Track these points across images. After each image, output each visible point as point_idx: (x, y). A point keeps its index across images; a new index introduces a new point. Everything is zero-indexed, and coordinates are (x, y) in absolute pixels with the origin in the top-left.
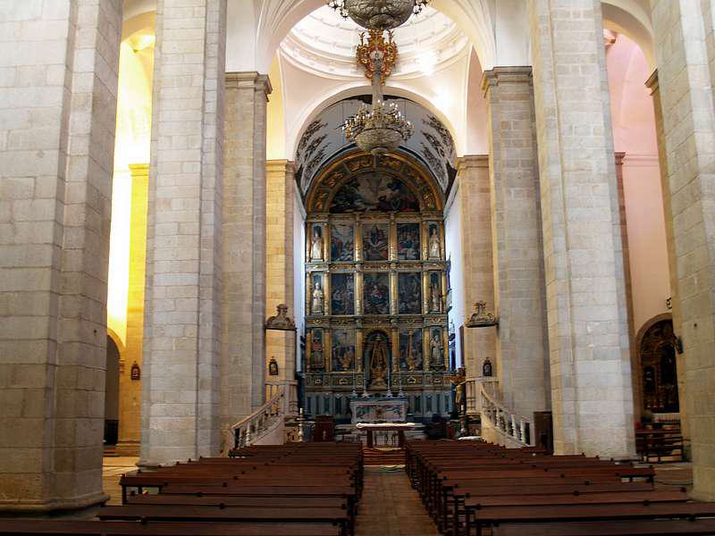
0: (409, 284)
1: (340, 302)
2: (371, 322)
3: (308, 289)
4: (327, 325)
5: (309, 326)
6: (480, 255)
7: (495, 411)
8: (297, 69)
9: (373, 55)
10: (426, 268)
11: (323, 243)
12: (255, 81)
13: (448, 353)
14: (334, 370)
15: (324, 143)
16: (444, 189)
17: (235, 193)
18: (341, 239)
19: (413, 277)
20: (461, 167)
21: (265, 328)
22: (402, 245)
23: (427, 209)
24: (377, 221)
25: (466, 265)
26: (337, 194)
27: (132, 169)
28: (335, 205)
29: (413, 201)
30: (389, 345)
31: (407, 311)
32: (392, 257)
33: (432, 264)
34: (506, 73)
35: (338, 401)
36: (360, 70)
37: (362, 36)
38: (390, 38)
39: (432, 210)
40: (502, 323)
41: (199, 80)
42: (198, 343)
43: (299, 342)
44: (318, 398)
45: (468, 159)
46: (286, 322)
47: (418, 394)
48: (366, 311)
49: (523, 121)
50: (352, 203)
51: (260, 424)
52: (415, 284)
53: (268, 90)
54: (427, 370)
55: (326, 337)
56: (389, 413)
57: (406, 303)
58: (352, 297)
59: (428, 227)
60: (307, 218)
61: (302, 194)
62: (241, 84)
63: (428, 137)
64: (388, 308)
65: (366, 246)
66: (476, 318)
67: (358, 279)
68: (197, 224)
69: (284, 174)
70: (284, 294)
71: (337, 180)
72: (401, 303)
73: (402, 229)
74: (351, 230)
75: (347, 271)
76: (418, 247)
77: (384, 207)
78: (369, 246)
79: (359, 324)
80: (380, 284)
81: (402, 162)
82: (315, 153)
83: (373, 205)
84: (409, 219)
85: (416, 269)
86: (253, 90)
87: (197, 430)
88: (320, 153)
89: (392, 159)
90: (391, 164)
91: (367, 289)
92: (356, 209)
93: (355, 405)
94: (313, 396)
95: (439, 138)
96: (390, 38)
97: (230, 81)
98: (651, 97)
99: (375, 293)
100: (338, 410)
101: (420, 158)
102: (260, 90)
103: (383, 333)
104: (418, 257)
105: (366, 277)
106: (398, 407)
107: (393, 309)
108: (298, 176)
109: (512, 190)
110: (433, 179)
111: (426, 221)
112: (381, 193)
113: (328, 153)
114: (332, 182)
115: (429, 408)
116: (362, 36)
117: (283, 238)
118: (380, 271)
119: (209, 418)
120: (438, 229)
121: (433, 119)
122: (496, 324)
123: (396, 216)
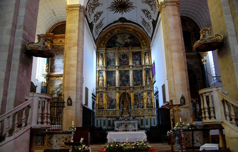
1: (110, 82)
44: (101, 120)
55: (104, 95)
57: (136, 82)
63: (144, 11)
71: (109, 36)
78: (121, 60)
82: (99, 21)
94: (99, 119)
112: (126, 41)
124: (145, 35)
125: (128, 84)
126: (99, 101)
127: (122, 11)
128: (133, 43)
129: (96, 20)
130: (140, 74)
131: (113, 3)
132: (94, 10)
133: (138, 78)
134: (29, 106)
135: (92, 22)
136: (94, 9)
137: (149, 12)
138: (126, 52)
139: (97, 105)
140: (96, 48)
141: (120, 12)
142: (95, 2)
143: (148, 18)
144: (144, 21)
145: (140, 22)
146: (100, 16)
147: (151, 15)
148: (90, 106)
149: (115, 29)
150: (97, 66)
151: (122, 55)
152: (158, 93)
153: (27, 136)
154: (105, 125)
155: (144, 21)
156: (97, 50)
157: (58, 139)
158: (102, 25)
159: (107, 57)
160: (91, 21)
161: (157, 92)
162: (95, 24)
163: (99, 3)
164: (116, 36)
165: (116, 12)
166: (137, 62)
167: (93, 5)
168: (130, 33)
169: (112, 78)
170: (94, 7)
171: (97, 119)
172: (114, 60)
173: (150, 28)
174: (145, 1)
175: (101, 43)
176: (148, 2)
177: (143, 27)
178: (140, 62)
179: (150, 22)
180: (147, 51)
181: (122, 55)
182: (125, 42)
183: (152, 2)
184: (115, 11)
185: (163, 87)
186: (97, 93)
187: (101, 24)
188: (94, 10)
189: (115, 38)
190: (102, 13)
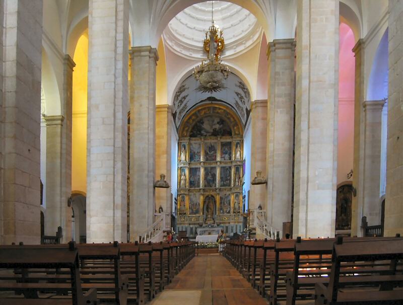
0: (226, 171)
1: (193, 181)
2: (207, 191)
3: (179, 175)
4: (187, 193)
5: (179, 193)
6: (261, 152)
7: (263, 226)
8: (172, 52)
10: (234, 164)
11: (186, 153)
12: (150, 52)
13: (241, 205)
14: (190, 214)
15: (187, 99)
16: (244, 123)
18: (195, 150)
19: (227, 169)
20: (253, 107)
21: (155, 187)
22: (223, 153)
23: (235, 134)
24: (211, 141)
26: (193, 128)
29: (229, 130)
30: (215, 202)
31: (224, 185)
32: (218, 159)
33: (236, 162)
34: (280, 43)
35: (192, 229)
37: (206, 34)
38: (221, 35)
39: (237, 134)
40: (269, 182)
41: (113, 33)
42: (114, 185)
43: (174, 200)
45: (257, 102)
46: (164, 183)
47: (227, 225)
48: (205, 186)
50: (200, 132)
51: (151, 234)
52: (228, 172)
53: (156, 59)
54: (232, 214)
55: (187, 198)
58: (199, 179)
59: (235, 144)
60: (179, 140)
61: (176, 127)
62: (143, 53)
63: (238, 94)
64: (215, 184)
65: (206, 154)
66: (257, 179)
67: (202, 171)
68: (113, 118)
69: (166, 112)
71: (193, 120)
72: (221, 181)
73: (223, 145)
74: (198, 145)
75: (196, 167)
76: (230, 154)
77: (215, 134)
79: (202, 192)
81: (224, 110)
82: (183, 105)
83: (210, 133)
84: (227, 139)
85: (229, 165)
86: (148, 57)
87: (114, 230)
88: (185, 105)
89: (220, 109)
90: (219, 111)
91: (206, 174)
92: (202, 135)
93: (199, 230)
95: (243, 94)
96: (221, 35)
97: (135, 53)
98: (354, 58)
99: (209, 177)
100: (191, 232)
101: (234, 108)
102: (152, 57)
103: (212, 196)
104: (230, 158)
105: (206, 169)
106: (218, 231)
108: (174, 115)
110: (240, 120)
111: (235, 140)
112: (214, 127)
113: (190, 105)
114: (191, 121)
115: (232, 231)
116: (206, 34)
118: (212, 166)
119: (120, 224)
120: (240, 144)
121: (240, 83)
122: (266, 183)
123: (221, 138)
126: (180, 206)
161: (245, 196)
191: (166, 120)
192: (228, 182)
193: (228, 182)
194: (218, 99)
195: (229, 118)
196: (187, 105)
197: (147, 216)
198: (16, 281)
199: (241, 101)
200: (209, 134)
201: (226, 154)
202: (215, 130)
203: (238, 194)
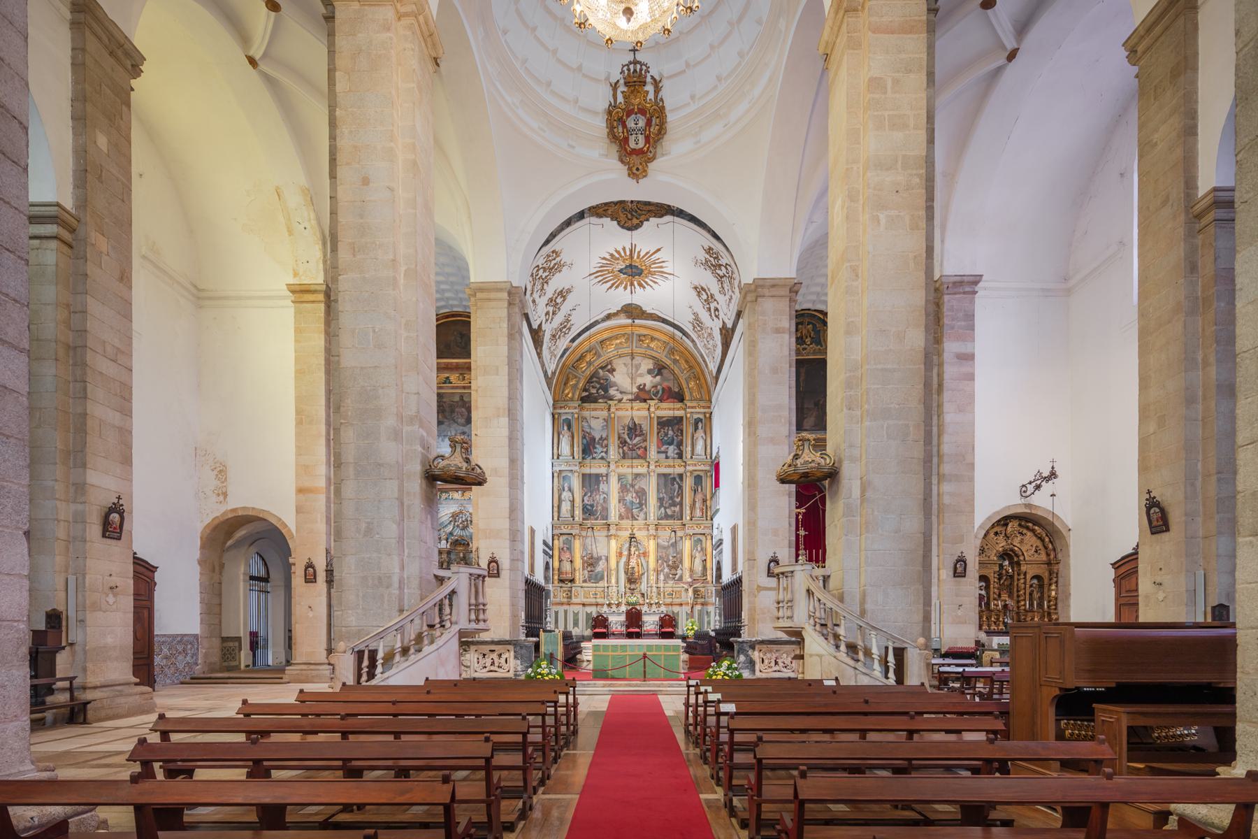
1: (592, 506)
5: (556, 532)
9: (630, 123)
14: (585, 581)
15: (571, 300)
17: (361, 216)
18: (593, 433)
19: (674, 479)
25: (749, 435)
26: (589, 381)
27: (293, 292)
28: (587, 393)
36: (614, 145)
43: (539, 547)
44: (566, 612)
49: (912, 76)
50: (606, 390)
55: (577, 544)
56: (567, 567)
57: (665, 508)
61: (545, 373)
63: (699, 290)
66: (799, 462)
70: (507, 470)
71: (590, 364)
72: (660, 508)
78: (626, 442)
80: (636, 487)
82: (559, 318)
85: (680, 470)
94: (561, 609)
104: (680, 456)
107: (652, 515)
109: (882, 217)
111: (692, 410)
112: (640, 381)
117: (506, 394)
118: (636, 471)
124: (699, 364)
125: (642, 515)
126: (560, 561)
127: (632, 284)
128: (663, 389)
129: (553, 314)
130: (676, 486)
131: (604, 258)
132: (545, 285)
133: (671, 498)
134: (453, 592)
135: (540, 326)
136: (546, 281)
137: (712, 297)
138: (640, 418)
139: (556, 572)
140: (551, 402)
141: (625, 288)
142: (551, 261)
143: (711, 315)
144: (697, 319)
145: (685, 321)
146: (564, 301)
147: (719, 307)
148: (539, 578)
149: (610, 339)
150: (555, 457)
151: (628, 426)
152: (721, 544)
153: (454, 644)
154: (578, 627)
155: (697, 322)
156: (554, 408)
157: (481, 657)
158: (569, 329)
159: (583, 431)
160: (538, 322)
161: (720, 542)
162: (548, 329)
163: (562, 263)
164: (610, 363)
165: (613, 288)
166: (671, 448)
167: (544, 271)
168: (654, 354)
169: (598, 496)
170: (546, 277)
171: (555, 608)
172: (605, 442)
173: (715, 346)
174: (704, 262)
175: (565, 384)
176: (713, 266)
177: (695, 339)
178: (680, 449)
179: (716, 325)
180: (701, 416)
181: (628, 426)
182: (637, 385)
183: (723, 268)
184: (609, 284)
185: (734, 530)
186: (556, 537)
187: (565, 326)
188: (545, 285)
189: (608, 371)
190: (569, 291)
191: (505, 325)
192: (677, 509)
193: (677, 509)
194: (649, 311)
195: (675, 361)
196: (573, 319)
197: (395, 579)
198: (149, 741)
199: (709, 309)
200: (630, 397)
201: (670, 444)
202: (641, 388)
203: (703, 538)
